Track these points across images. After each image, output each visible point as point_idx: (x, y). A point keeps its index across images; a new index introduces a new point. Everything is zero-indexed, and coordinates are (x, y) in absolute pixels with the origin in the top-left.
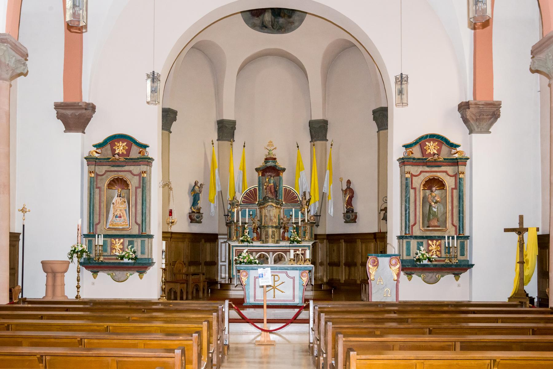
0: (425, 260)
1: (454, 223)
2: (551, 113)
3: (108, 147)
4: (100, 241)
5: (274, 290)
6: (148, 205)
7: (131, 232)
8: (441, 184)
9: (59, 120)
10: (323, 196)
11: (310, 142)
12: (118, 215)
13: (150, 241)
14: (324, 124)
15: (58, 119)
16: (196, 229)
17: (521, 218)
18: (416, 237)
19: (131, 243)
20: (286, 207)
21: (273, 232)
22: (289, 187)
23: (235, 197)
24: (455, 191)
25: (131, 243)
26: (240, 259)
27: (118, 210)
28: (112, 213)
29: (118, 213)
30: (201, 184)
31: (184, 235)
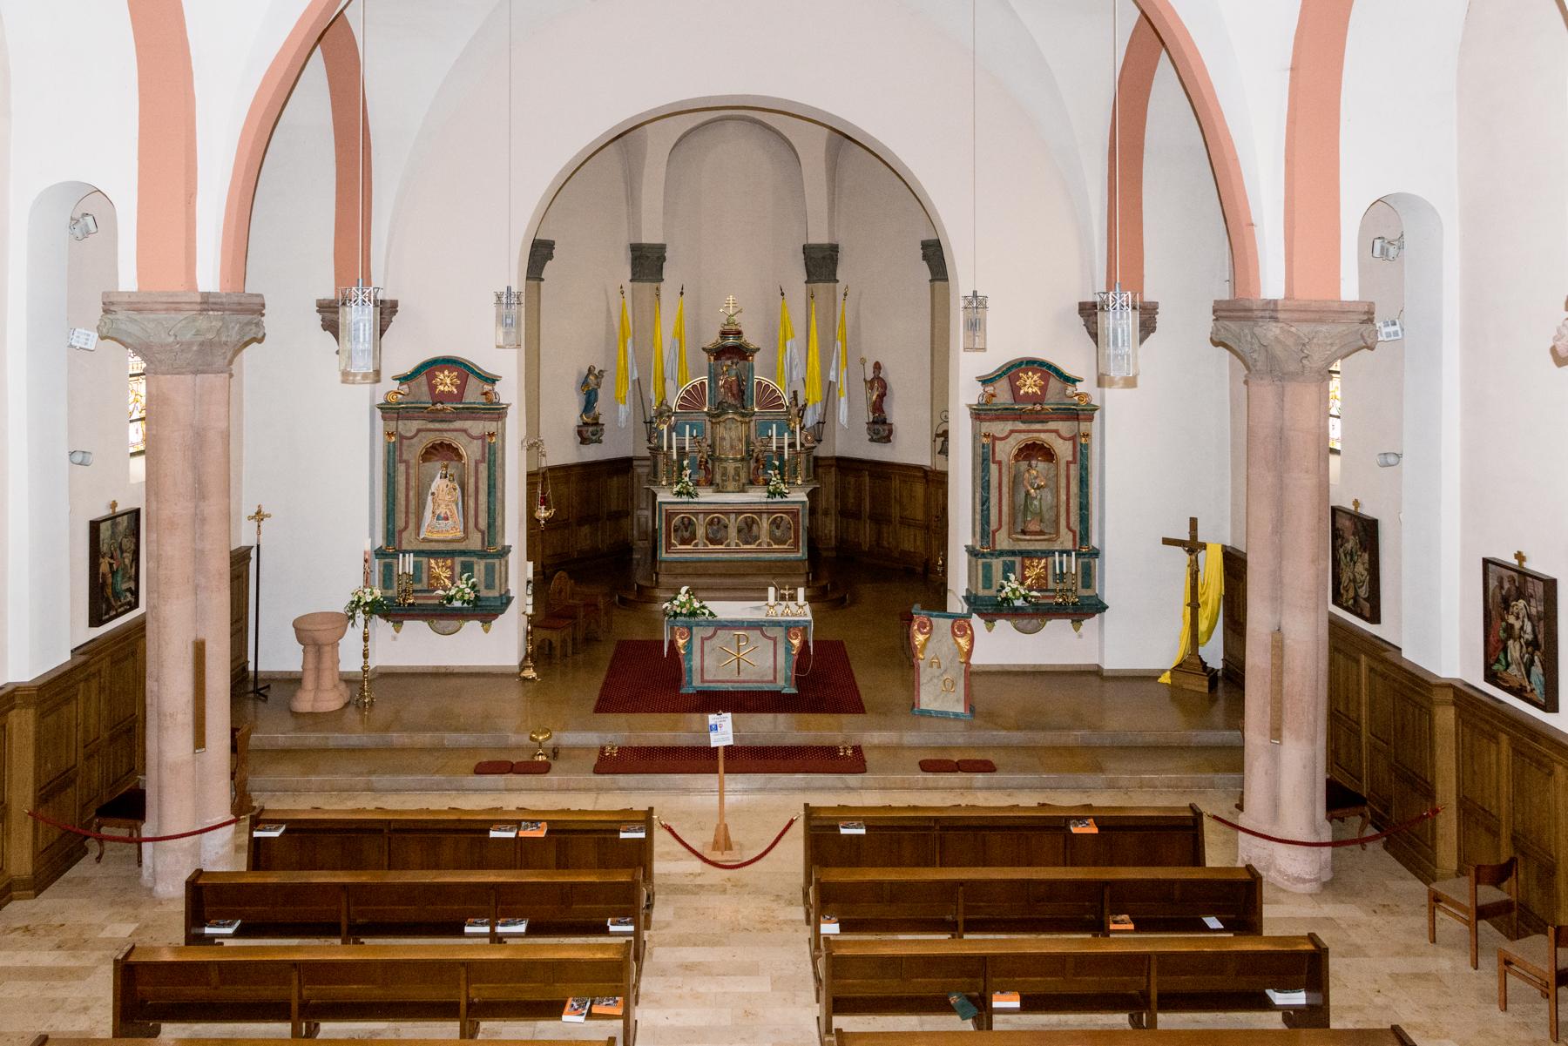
0: (1018, 599)
1: (1071, 525)
2: (1250, 415)
3: (423, 379)
4: (406, 564)
5: (739, 661)
6: (499, 494)
7: (467, 545)
8: (1048, 454)
9: (327, 332)
10: (829, 388)
11: (806, 282)
12: (442, 515)
13: (503, 562)
14: (832, 253)
15: (325, 330)
16: (592, 453)
17: (1193, 523)
18: (1002, 553)
19: (467, 567)
20: (761, 417)
21: (736, 469)
22: (766, 380)
23: (664, 402)
24: (1072, 466)
25: (467, 567)
26: (675, 608)
27: (443, 506)
28: (431, 511)
29: (442, 511)
30: (601, 371)
31: (566, 469)
